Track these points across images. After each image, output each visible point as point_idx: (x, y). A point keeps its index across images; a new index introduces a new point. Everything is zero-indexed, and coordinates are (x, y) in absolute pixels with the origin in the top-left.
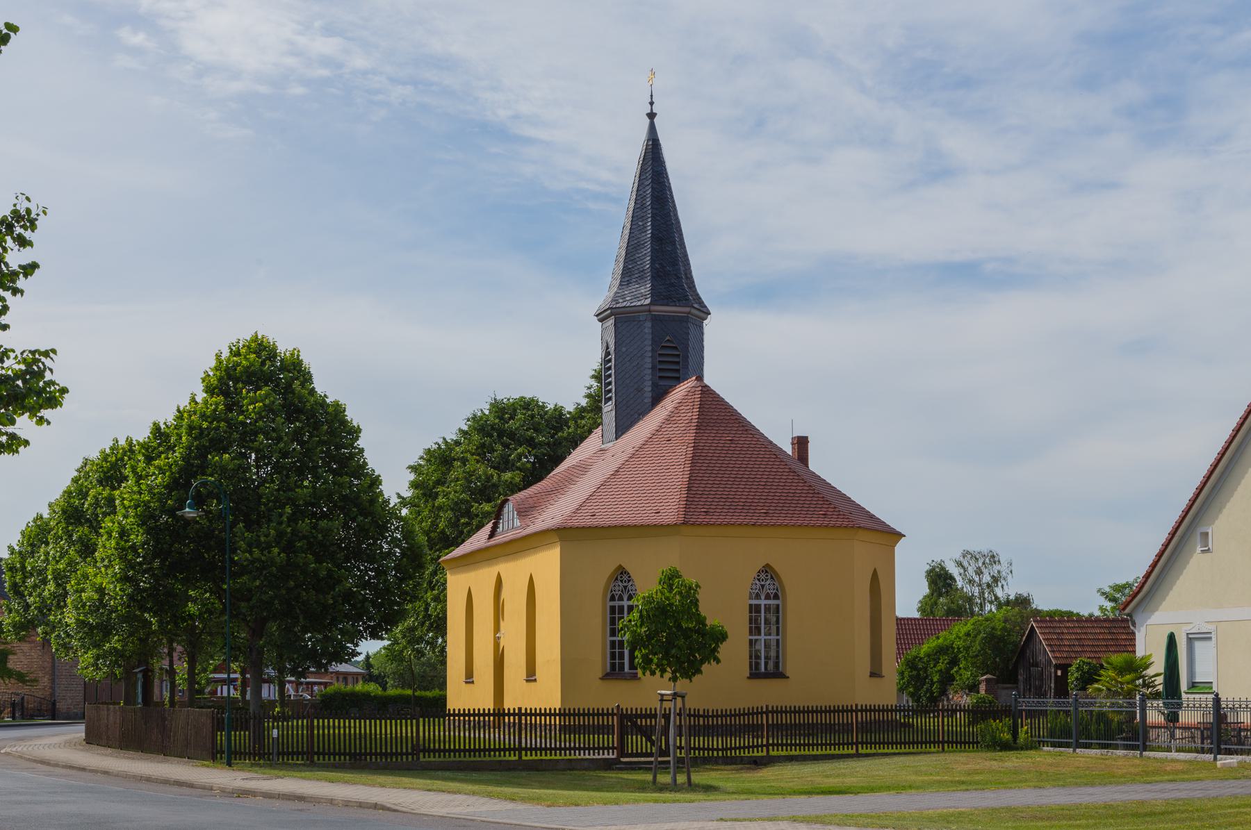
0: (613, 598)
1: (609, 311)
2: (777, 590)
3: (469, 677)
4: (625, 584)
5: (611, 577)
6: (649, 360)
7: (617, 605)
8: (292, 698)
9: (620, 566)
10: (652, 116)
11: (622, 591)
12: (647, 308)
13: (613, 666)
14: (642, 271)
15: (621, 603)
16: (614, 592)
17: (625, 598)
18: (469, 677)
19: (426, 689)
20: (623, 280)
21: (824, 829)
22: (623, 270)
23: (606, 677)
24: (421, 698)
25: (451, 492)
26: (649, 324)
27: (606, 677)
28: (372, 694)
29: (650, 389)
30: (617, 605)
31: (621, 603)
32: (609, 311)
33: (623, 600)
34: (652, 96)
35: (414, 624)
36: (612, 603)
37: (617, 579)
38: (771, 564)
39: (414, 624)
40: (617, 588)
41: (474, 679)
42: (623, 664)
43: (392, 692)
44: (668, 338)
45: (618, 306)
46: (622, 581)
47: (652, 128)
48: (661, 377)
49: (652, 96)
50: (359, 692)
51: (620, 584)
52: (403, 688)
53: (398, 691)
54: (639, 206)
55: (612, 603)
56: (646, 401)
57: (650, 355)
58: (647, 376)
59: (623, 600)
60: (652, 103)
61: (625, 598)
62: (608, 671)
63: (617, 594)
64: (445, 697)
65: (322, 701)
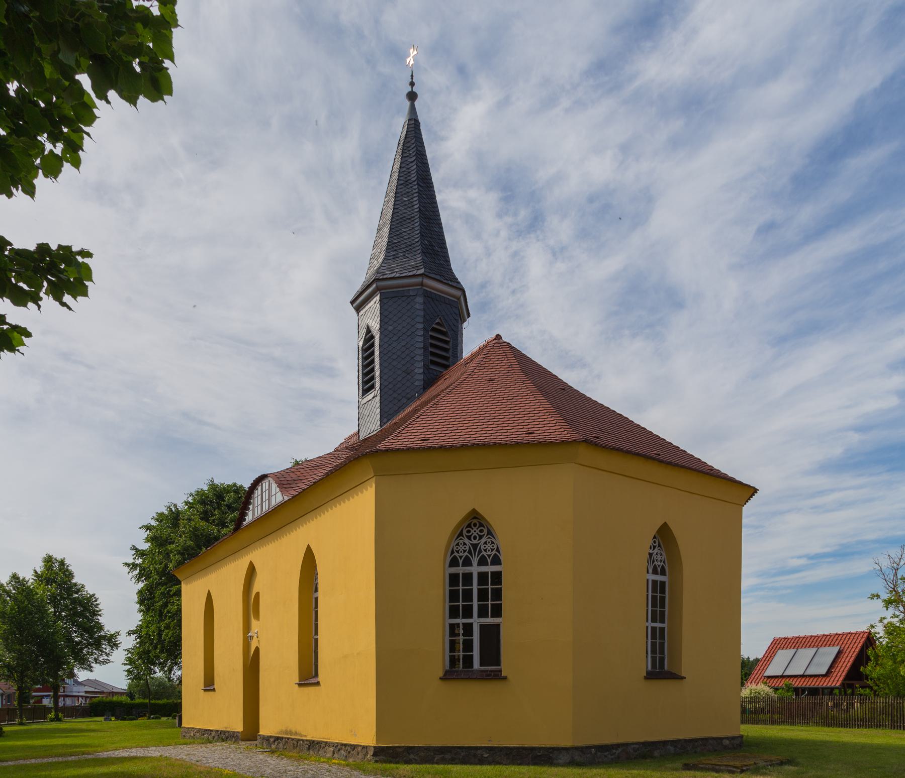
0: (454, 563)
1: (374, 286)
2: (664, 562)
3: (209, 684)
4: (475, 542)
5: (453, 532)
6: (421, 339)
7: (461, 572)
8: (83, 705)
9: (474, 511)
10: (412, 96)
11: (470, 552)
12: (419, 280)
13: (453, 661)
14: (410, 245)
15: (467, 569)
16: (456, 554)
17: (475, 561)
18: (209, 684)
19: (158, 699)
20: (389, 254)
21: (384, 772)
22: (388, 245)
23: (449, 675)
24: (155, 704)
25: (182, 540)
26: (420, 300)
27: (449, 675)
28: (124, 703)
29: (421, 371)
30: (461, 572)
31: (467, 569)
32: (374, 286)
33: (471, 565)
34: (412, 76)
35: (148, 648)
36: (454, 570)
37: (461, 534)
38: (668, 523)
39: (148, 648)
40: (461, 548)
41: (215, 686)
42: (471, 658)
43: (137, 701)
44: (438, 320)
45: (385, 277)
46: (469, 538)
47: (413, 109)
48: (432, 362)
49: (412, 76)
50: (115, 701)
51: (467, 541)
52: (144, 699)
53: (141, 701)
54: (402, 182)
55: (454, 570)
56: (416, 384)
57: (422, 333)
58: (417, 356)
59: (471, 565)
60: (412, 84)
61: (475, 561)
62: (448, 668)
63: (461, 557)
64: (181, 703)
65: (91, 707)
